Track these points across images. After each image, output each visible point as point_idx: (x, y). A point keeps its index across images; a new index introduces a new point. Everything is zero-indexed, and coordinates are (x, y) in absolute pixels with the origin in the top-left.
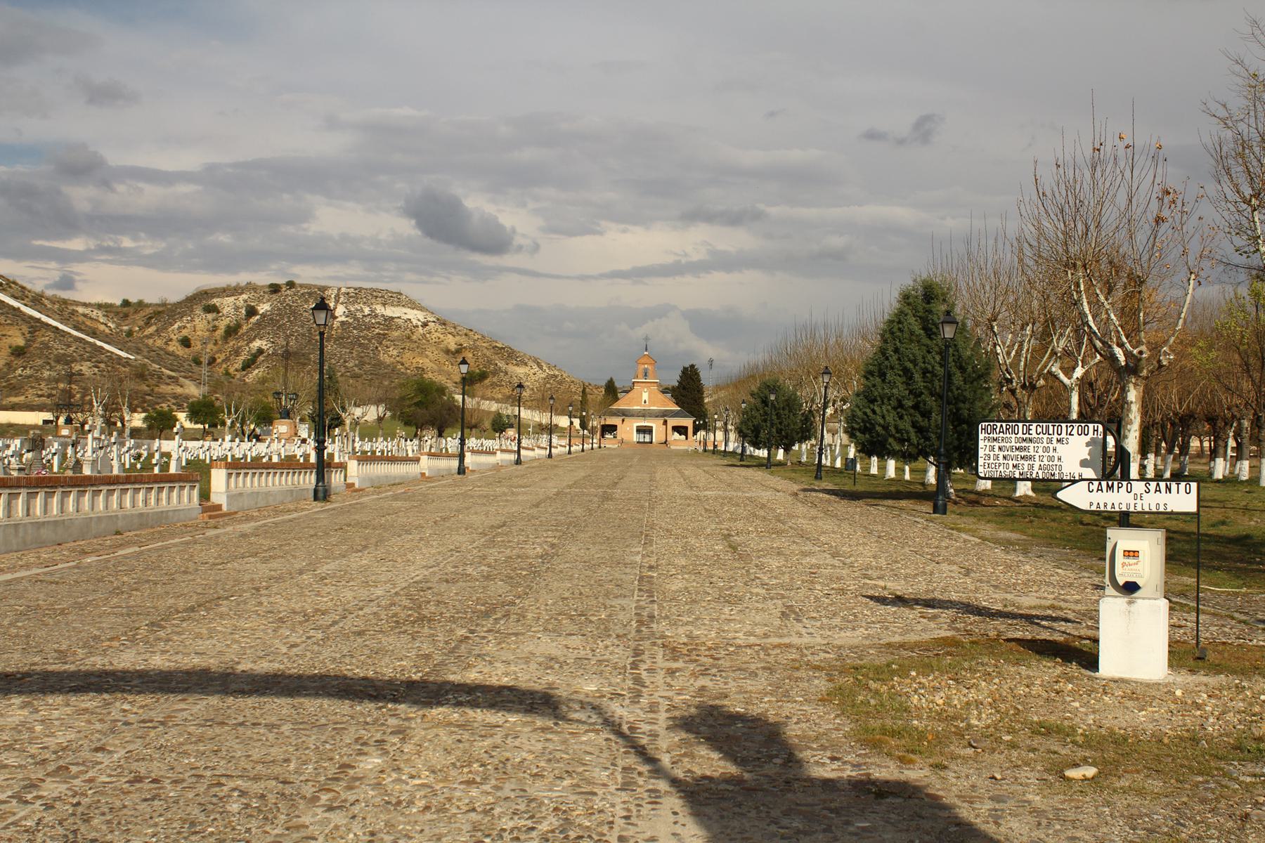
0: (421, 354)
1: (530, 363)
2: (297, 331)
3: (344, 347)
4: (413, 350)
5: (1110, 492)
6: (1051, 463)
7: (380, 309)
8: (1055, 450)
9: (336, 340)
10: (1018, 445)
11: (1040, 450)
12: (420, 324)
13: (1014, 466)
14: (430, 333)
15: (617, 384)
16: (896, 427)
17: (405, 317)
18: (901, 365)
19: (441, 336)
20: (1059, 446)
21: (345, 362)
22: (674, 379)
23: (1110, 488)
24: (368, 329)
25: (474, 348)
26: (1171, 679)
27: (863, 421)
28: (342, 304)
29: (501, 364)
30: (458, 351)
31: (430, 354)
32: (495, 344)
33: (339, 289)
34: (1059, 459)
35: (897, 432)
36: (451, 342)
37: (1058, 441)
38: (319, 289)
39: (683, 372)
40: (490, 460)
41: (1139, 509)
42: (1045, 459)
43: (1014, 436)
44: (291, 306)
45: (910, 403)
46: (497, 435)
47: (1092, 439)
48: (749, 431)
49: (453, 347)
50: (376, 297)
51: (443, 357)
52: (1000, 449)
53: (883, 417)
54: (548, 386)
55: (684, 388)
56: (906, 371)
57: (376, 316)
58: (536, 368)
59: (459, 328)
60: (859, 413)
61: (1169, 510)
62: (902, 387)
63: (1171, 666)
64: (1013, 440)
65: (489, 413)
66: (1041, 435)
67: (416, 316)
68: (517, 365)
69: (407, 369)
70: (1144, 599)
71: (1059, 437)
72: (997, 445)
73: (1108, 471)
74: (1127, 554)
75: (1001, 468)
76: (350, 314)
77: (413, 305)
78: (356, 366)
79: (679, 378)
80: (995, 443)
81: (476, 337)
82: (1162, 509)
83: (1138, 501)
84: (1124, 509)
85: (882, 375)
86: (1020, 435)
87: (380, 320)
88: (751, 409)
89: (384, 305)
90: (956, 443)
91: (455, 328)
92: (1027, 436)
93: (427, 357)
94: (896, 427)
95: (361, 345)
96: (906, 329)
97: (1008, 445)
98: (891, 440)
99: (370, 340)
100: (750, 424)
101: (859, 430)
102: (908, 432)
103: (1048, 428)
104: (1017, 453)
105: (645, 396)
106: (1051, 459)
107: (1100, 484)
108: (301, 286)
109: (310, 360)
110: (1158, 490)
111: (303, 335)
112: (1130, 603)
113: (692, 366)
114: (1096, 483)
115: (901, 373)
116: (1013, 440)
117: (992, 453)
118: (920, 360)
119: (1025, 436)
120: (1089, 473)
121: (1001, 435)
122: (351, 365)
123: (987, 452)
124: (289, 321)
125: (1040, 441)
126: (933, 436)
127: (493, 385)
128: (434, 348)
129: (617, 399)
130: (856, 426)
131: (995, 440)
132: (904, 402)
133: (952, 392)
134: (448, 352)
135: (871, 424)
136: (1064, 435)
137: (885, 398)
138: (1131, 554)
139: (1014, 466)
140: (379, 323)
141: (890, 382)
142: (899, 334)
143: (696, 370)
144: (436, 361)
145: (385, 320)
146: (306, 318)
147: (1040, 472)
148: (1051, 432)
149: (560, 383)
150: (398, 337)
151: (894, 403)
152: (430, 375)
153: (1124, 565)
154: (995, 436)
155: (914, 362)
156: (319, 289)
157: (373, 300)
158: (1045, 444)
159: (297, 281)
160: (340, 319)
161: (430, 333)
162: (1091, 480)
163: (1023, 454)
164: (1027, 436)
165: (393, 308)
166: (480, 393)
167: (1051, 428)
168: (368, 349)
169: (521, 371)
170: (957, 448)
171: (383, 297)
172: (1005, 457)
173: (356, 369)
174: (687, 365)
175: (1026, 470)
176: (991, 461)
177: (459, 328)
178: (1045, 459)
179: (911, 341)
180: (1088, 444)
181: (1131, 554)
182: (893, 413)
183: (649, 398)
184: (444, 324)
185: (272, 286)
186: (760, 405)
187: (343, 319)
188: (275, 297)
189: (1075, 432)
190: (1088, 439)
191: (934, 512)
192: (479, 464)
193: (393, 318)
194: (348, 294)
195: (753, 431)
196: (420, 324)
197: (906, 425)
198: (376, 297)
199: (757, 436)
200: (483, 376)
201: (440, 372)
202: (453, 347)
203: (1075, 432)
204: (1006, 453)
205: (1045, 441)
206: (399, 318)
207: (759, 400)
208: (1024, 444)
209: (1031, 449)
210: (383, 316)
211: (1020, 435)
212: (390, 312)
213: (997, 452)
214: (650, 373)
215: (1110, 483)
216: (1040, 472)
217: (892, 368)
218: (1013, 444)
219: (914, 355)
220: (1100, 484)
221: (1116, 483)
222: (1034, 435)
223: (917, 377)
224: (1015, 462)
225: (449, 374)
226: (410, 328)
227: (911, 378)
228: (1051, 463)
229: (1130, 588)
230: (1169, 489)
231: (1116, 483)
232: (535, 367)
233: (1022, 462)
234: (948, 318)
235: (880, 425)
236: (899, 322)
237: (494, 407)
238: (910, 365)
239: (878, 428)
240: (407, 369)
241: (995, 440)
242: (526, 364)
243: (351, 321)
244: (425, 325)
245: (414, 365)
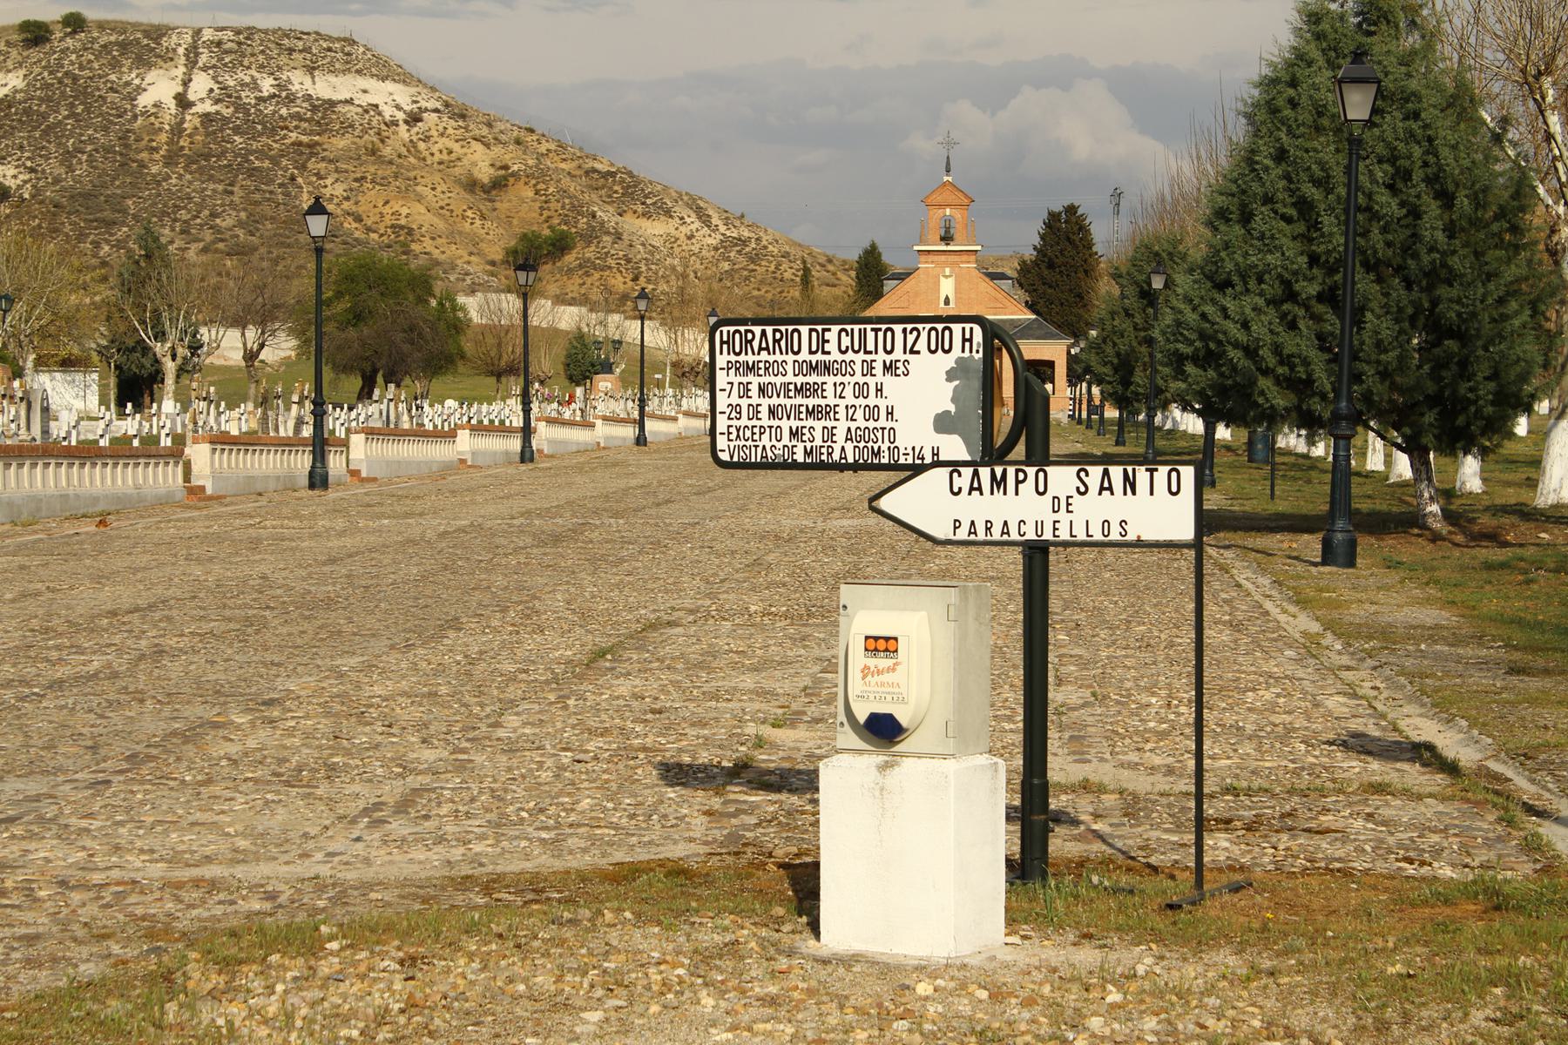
0: (406, 193)
1: (680, 210)
2: (91, 140)
3: (211, 178)
4: (383, 183)
5: (998, 495)
6: (871, 424)
7: (300, 82)
8: (879, 390)
9: (190, 161)
10: (800, 380)
11: (848, 392)
12: (400, 116)
13: (794, 434)
14: (427, 139)
15: (887, 258)
16: (1277, 350)
17: (363, 100)
18: (1292, 192)
19: (456, 147)
20: (889, 381)
21: (214, 215)
22: (1026, 239)
23: (999, 483)
24: (273, 132)
25: (538, 176)
26: (1007, 955)
27: (1203, 336)
28: (205, 69)
29: (606, 214)
30: (498, 185)
31: (426, 191)
32: (590, 164)
33: (198, 32)
34: (890, 413)
35: (1281, 363)
36: (480, 160)
37: (889, 368)
38: (147, 34)
39: (1048, 225)
40: (438, 452)
41: (1064, 535)
42: (859, 415)
43: (790, 358)
44: (75, 79)
45: (1313, 289)
46: (579, 391)
47: (959, 361)
48: (1107, 370)
49: (484, 173)
50: (291, 51)
51: (459, 200)
52: (762, 390)
53: (1245, 325)
54: (726, 266)
55: (1051, 266)
56: (1304, 206)
57: (291, 99)
58: (694, 223)
59: (500, 126)
60: (1191, 317)
61: (1131, 537)
62: (1291, 248)
63: (1012, 921)
64: (789, 368)
65: (553, 333)
66: (850, 356)
67: (390, 97)
68: (646, 215)
69: (369, 230)
70: (919, 756)
71: (888, 358)
72: (755, 381)
73: (999, 441)
74: (872, 643)
75: (766, 437)
76: (224, 95)
77: (384, 70)
78: (241, 224)
79: (1037, 241)
80: (750, 378)
81: (543, 149)
82: (1115, 536)
83: (1062, 516)
84: (1031, 535)
85: (1246, 218)
86: (804, 355)
87: (301, 108)
88: (1113, 314)
89: (311, 70)
90: (1431, 388)
91: (490, 125)
92: (819, 357)
93: (420, 199)
94: (1277, 350)
95: (252, 172)
96: (1304, 100)
97: (779, 380)
98: (1264, 383)
99: (275, 161)
100: (1109, 350)
101: (1195, 359)
102: (1306, 362)
103: (863, 333)
104: (799, 400)
105: (947, 287)
106: (872, 412)
107: (976, 473)
108: (102, 26)
109: (124, 212)
110: (975, 488)
111: (108, 150)
112: (884, 767)
113: (1071, 210)
114: (967, 472)
115: (1292, 212)
116: (789, 368)
117: (744, 402)
118: (1338, 175)
119: (814, 358)
120: (954, 447)
121: (764, 356)
122: (229, 222)
123: (735, 400)
124: (73, 115)
125: (845, 368)
126: (1369, 370)
127: (586, 267)
128: (437, 178)
129: (878, 295)
130: (1184, 349)
131: (751, 369)
132: (1297, 287)
133: (1416, 256)
134: (472, 185)
135: (1220, 343)
136: (898, 354)
137: (1251, 276)
138: (881, 645)
139: (794, 434)
140: (298, 117)
141: (1262, 237)
142: (1287, 112)
143: (1082, 218)
144: (443, 210)
145: (314, 109)
146: (113, 106)
147: (849, 447)
148: (870, 347)
149: (754, 259)
150: (347, 149)
151: (1272, 288)
152: (428, 244)
153: (866, 671)
154: (750, 358)
155: (1324, 183)
156: (147, 34)
157: (284, 59)
158: (859, 378)
159: (91, 14)
160: (200, 108)
161: (427, 139)
162: (955, 466)
163: (811, 402)
164: (819, 357)
165: (332, 78)
166: (553, 289)
167: (871, 336)
168: (270, 182)
169: (655, 229)
170: (1434, 400)
171: (307, 50)
172: (772, 412)
173: (240, 232)
174: (1058, 208)
175: (818, 442)
176: (744, 421)
177: (500, 126)
178: (859, 415)
179: (1318, 129)
180: (951, 375)
181: (881, 645)
182: (1271, 314)
183: (957, 290)
184: (463, 117)
185: (26, 26)
186: (1133, 302)
187: (208, 107)
188: (34, 54)
189: (922, 345)
190: (948, 361)
191: (1324, 563)
192: (484, 453)
193: (332, 104)
194: (219, 44)
195: (1116, 370)
196: (400, 116)
197: (1301, 343)
198: (291, 51)
199: (1126, 382)
200: (560, 245)
201: (453, 236)
202: (484, 173)
203: (922, 345)
204: (775, 401)
205: (858, 368)
206: (349, 102)
207: (1131, 291)
208: (813, 378)
209: (829, 388)
210: (308, 97)
211: (804, 355)
212: (325, 87)
213: (755, 400)
214: (958, 232)
215: (999, 470)
216: (849, 447)
217: (1268, 200)
218: (790, 378)
219: (1322, 165)
220: (976, 473)
221: (1011, 471)
222: (836, 355)
223: (1328, 222)
224: (795, 424)
225: (474, 244)
226: (375, 124)
227: (1315, 225)
228: (871, 424)
229: (884, 730)
230: (1130, 484)
231: (1011, 471)
232: (692, 218)
233: (810, 422)
234: (1358, 71)
235: (1236, 345)
236: (1293, 83)
237: (568, 318)
238: (1310, 191)
239: (1234, 354)
240: (369, 230)
241: (751, 369)
242: (668, 213)
243: (227, 112)
244: (414, 119)
245: (388, 220)
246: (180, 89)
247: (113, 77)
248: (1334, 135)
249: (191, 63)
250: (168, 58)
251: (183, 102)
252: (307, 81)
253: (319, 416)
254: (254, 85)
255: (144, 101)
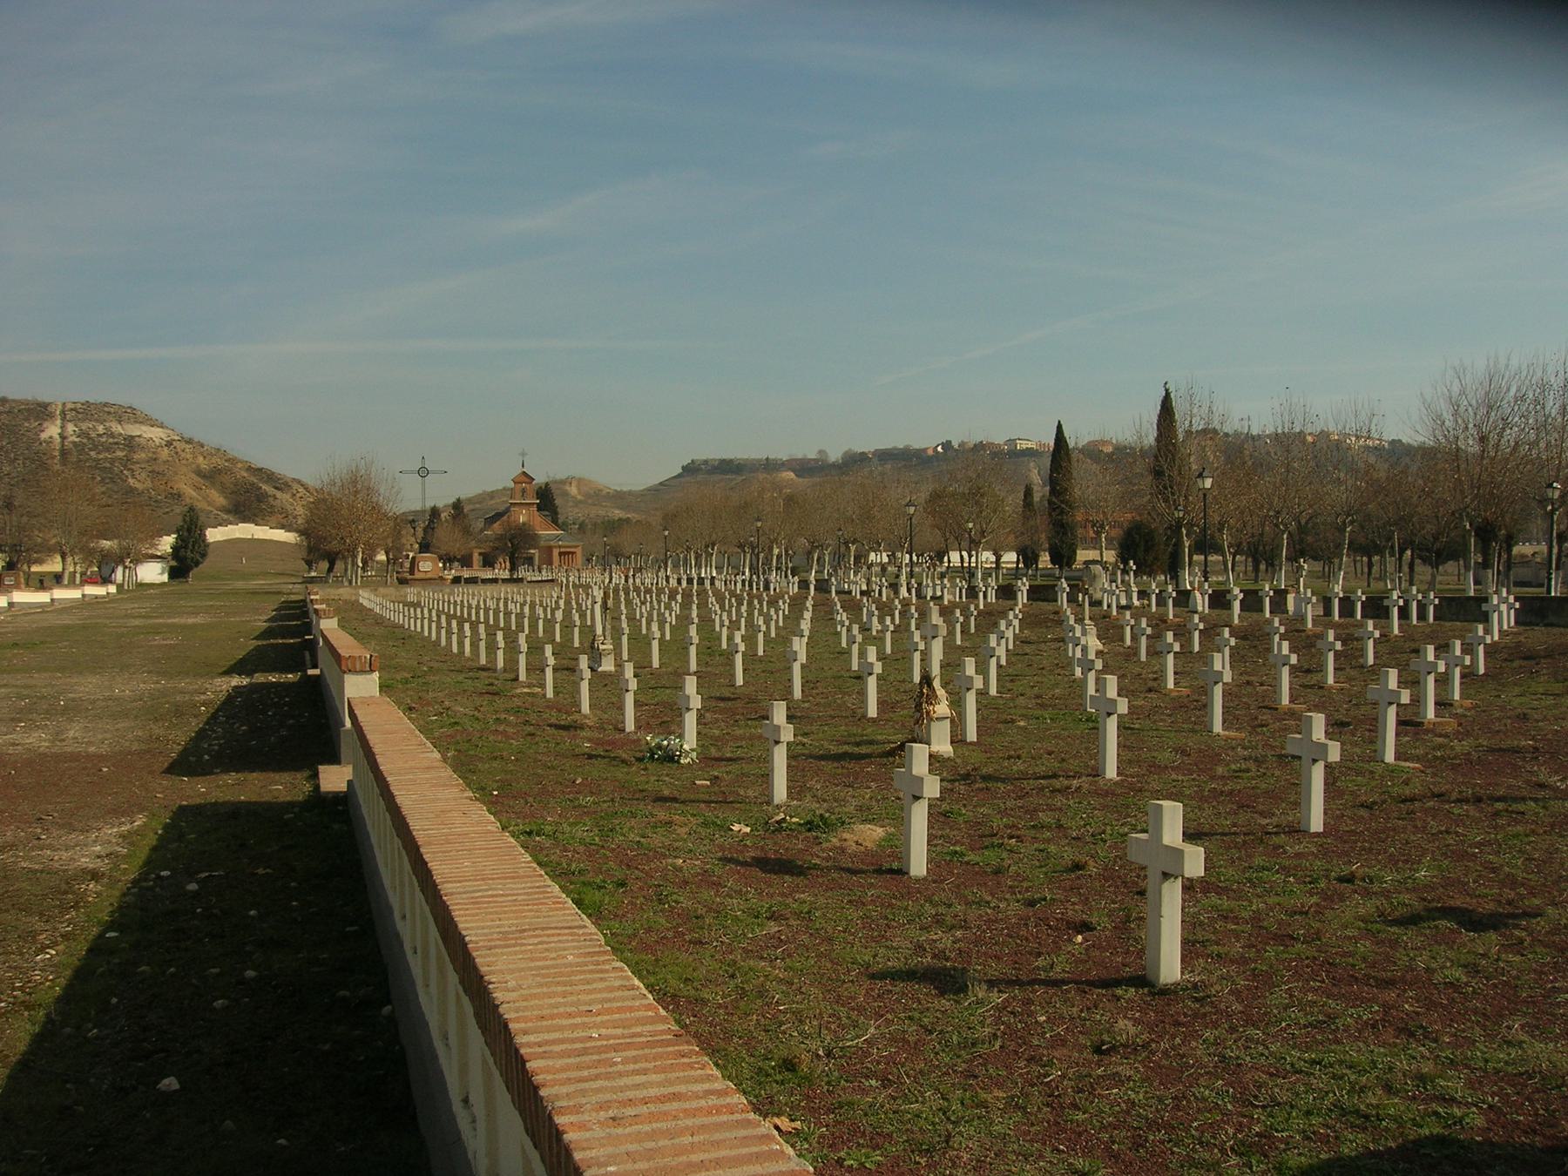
7: (117, 428)
28: (70, 421)
57: (112, 435)
67: (155, 434)
77: (153, 423)
160: (71, 439)
193: (133, 437)
246: (59, 431)
247: (27, 425)
248: (584, 900)
249: (64, 418)
250: (51, 416)
251: (63, 437)
252: (119, 427)
253: (998, 562)
254: (94, 429)
255: (44, 436)
